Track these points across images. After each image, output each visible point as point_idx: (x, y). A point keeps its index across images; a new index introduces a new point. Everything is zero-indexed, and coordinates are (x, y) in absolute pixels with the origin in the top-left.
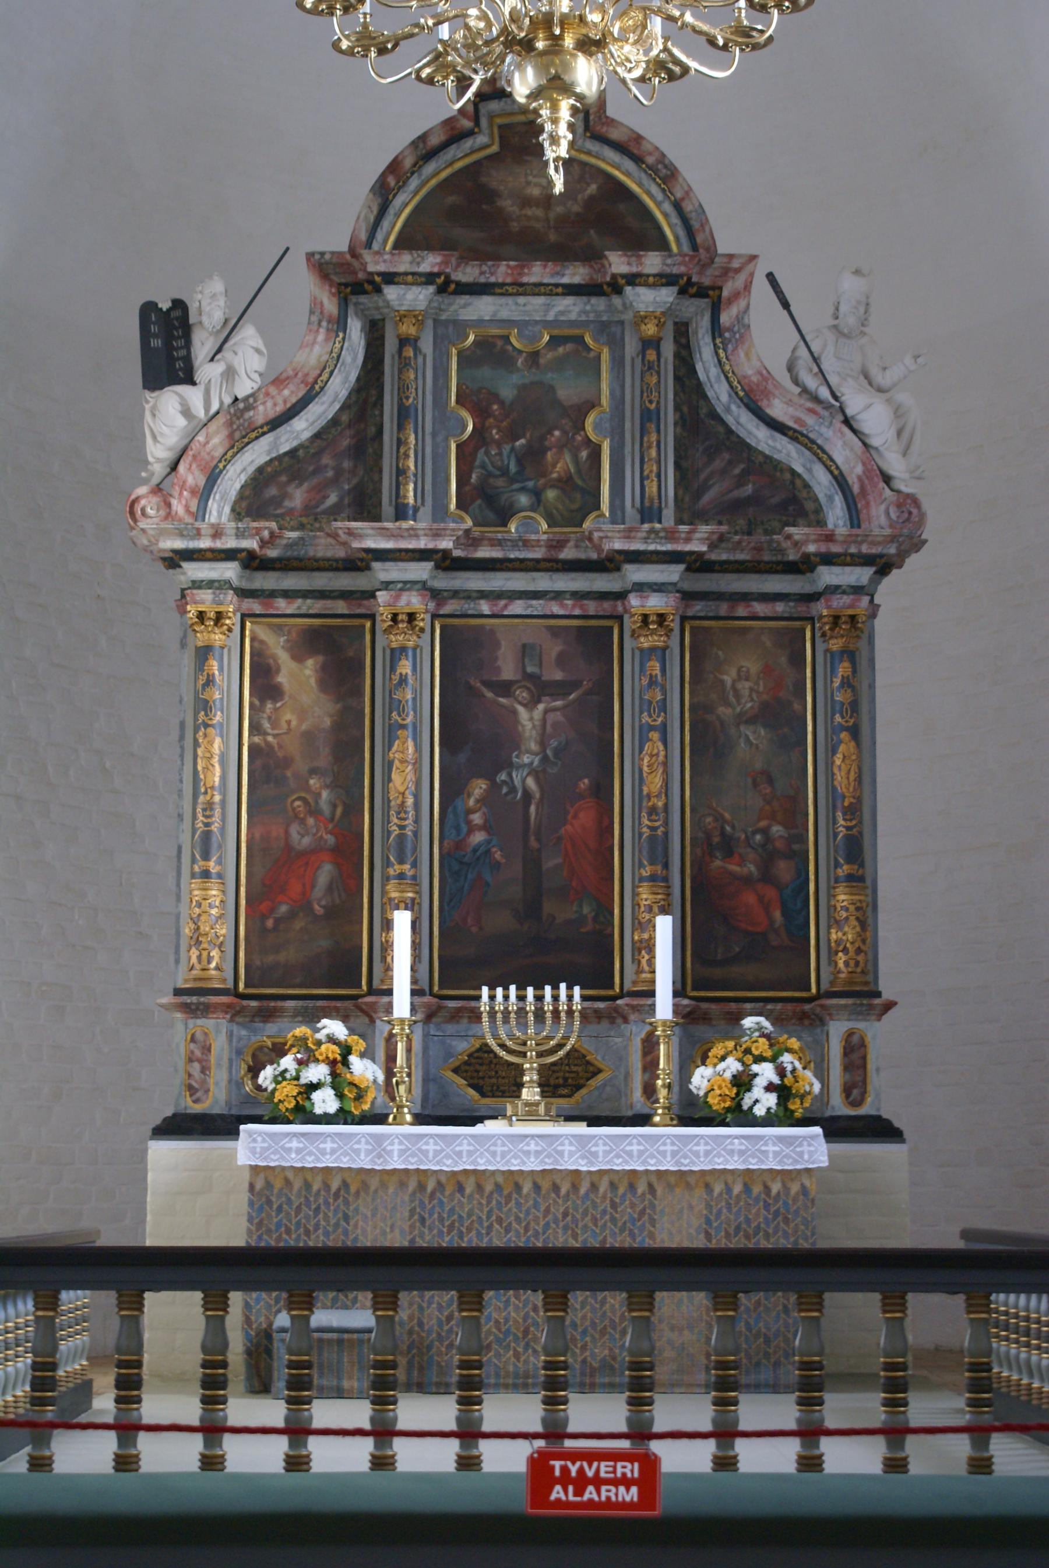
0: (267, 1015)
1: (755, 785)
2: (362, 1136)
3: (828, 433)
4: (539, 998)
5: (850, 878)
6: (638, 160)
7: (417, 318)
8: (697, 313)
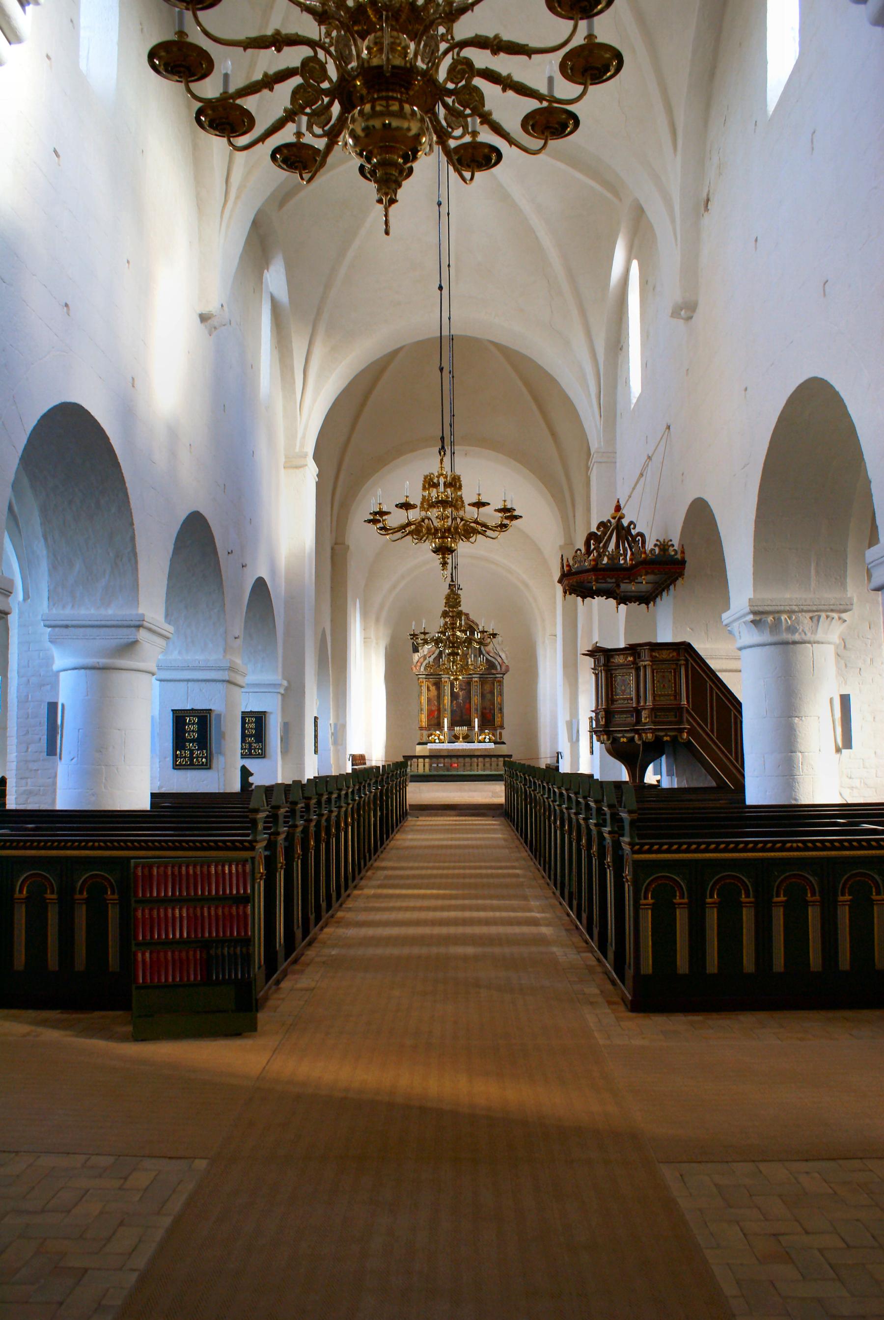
2: (440, 744)
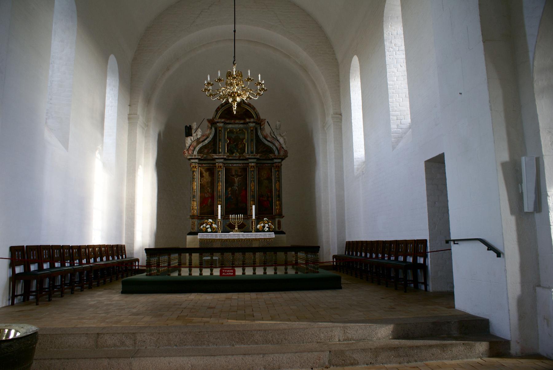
0: (202, 219)
2: (213, 234)
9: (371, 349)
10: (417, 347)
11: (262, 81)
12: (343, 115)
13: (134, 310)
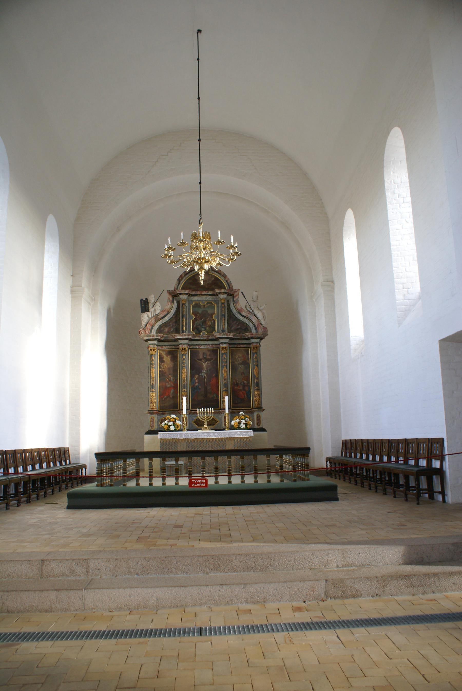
0: (163, 414)
1: (242, 374)
2: (178, 433)
3: (252, 317)
4: (207, 410)
5: (257, 389)
6: (220, 274)
7: (185, 300)
8: (230, 298)
9: (377, 577)
10: (435, 574)
11: (234, 243)
12: (335, 282)
13: (85, 531)
